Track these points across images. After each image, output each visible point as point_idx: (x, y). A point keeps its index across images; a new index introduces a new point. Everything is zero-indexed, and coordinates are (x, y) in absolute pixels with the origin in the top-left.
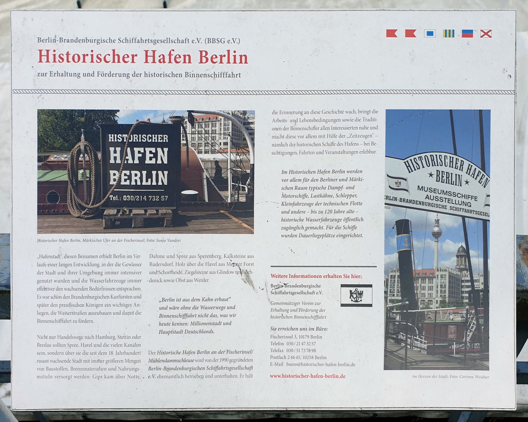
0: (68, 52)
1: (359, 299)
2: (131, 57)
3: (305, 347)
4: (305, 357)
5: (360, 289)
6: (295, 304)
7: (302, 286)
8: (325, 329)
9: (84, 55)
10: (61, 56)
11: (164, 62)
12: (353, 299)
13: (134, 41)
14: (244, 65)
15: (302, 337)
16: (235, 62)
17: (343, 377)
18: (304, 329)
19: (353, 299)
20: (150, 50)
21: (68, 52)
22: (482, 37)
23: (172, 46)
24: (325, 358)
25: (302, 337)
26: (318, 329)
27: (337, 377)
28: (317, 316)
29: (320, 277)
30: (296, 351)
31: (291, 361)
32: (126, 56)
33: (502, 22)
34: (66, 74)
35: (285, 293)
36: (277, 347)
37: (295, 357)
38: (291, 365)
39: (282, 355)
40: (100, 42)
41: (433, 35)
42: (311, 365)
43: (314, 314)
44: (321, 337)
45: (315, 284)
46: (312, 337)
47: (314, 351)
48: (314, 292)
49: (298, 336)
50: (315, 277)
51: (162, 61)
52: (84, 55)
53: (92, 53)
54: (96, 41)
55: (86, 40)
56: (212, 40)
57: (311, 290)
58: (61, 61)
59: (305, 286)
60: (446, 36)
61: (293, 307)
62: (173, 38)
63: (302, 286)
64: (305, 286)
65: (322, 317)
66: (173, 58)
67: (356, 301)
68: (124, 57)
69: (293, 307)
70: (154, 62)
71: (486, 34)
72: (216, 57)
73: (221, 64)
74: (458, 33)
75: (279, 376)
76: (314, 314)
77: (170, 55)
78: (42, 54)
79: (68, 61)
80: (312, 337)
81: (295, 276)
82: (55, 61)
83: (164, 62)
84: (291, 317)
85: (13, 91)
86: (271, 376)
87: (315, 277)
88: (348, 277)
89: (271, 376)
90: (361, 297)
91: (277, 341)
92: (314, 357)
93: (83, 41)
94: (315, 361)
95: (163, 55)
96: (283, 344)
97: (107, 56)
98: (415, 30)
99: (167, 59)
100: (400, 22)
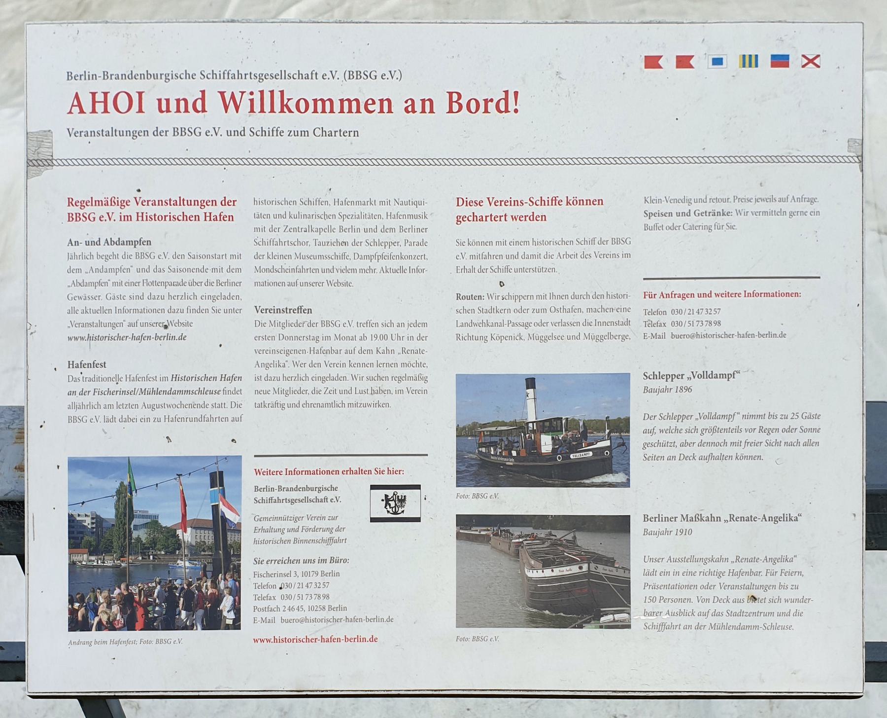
3: (312, 590)
4: (311, 609)
5: (400, 493)
6: (296, 519)
7: (307, 489)
8: (345, 561)
9: (486, 101)
11: (414, 111)
12: (390, 510)
13: (226, 76)
14: (428, 115)
15: (305, 574)
16: (272, 111)
17: (373, 640)
18: (310, 561)
19: (390, 510)
20: (99, 92)
22: (803, 66)
24: (345, 609)
25: (305, 574)
26: (333, 560)
27: (364, 640)
28: (331, 539)
29: (337, 472)
30: (296, 598)
31: (288, 615)
32: (370, 102)
33: (838, 44)
34: (113, 132)
35: (279, 500)
37: (296, 607)
38: (289, 621)
39: (272, 604)
40: (170, 77)
41: (722, 64)
42: (321, 620)
44: (338, 574)
45: (327, 486)
46: (323, 574)
47: (327, 597)
48: (326, 499)
49: (299, 574)
50: (328, 472)
51: (410, 109)
52: (486, 101)
54: (163, 77)
57: (321, 496)
59: (312, 489)
60: (744, 66)
61: (291, 525)
63: (307, 489)
64: (312, 489)
65: (339, 541)
67: (395, 513)
68: (366, 104)
69: (291, 525)
71: (811, 61)
73: (140, 114)
74: (765, 61)
75: (268, 641)
76: (326, 535)
78: (97, 100)
80: (323, 574)
81: (295, 472)
83: (414, 111)
84: (289, 541)
86: (256, 641)
87: (328, 472)
88: (382, 472)
89: (256, 641)
90: (402, 506)
92: (327, 608)
94: (330, 615)
95: (413, 101)
98: (661, 57)
100: (669, 42)
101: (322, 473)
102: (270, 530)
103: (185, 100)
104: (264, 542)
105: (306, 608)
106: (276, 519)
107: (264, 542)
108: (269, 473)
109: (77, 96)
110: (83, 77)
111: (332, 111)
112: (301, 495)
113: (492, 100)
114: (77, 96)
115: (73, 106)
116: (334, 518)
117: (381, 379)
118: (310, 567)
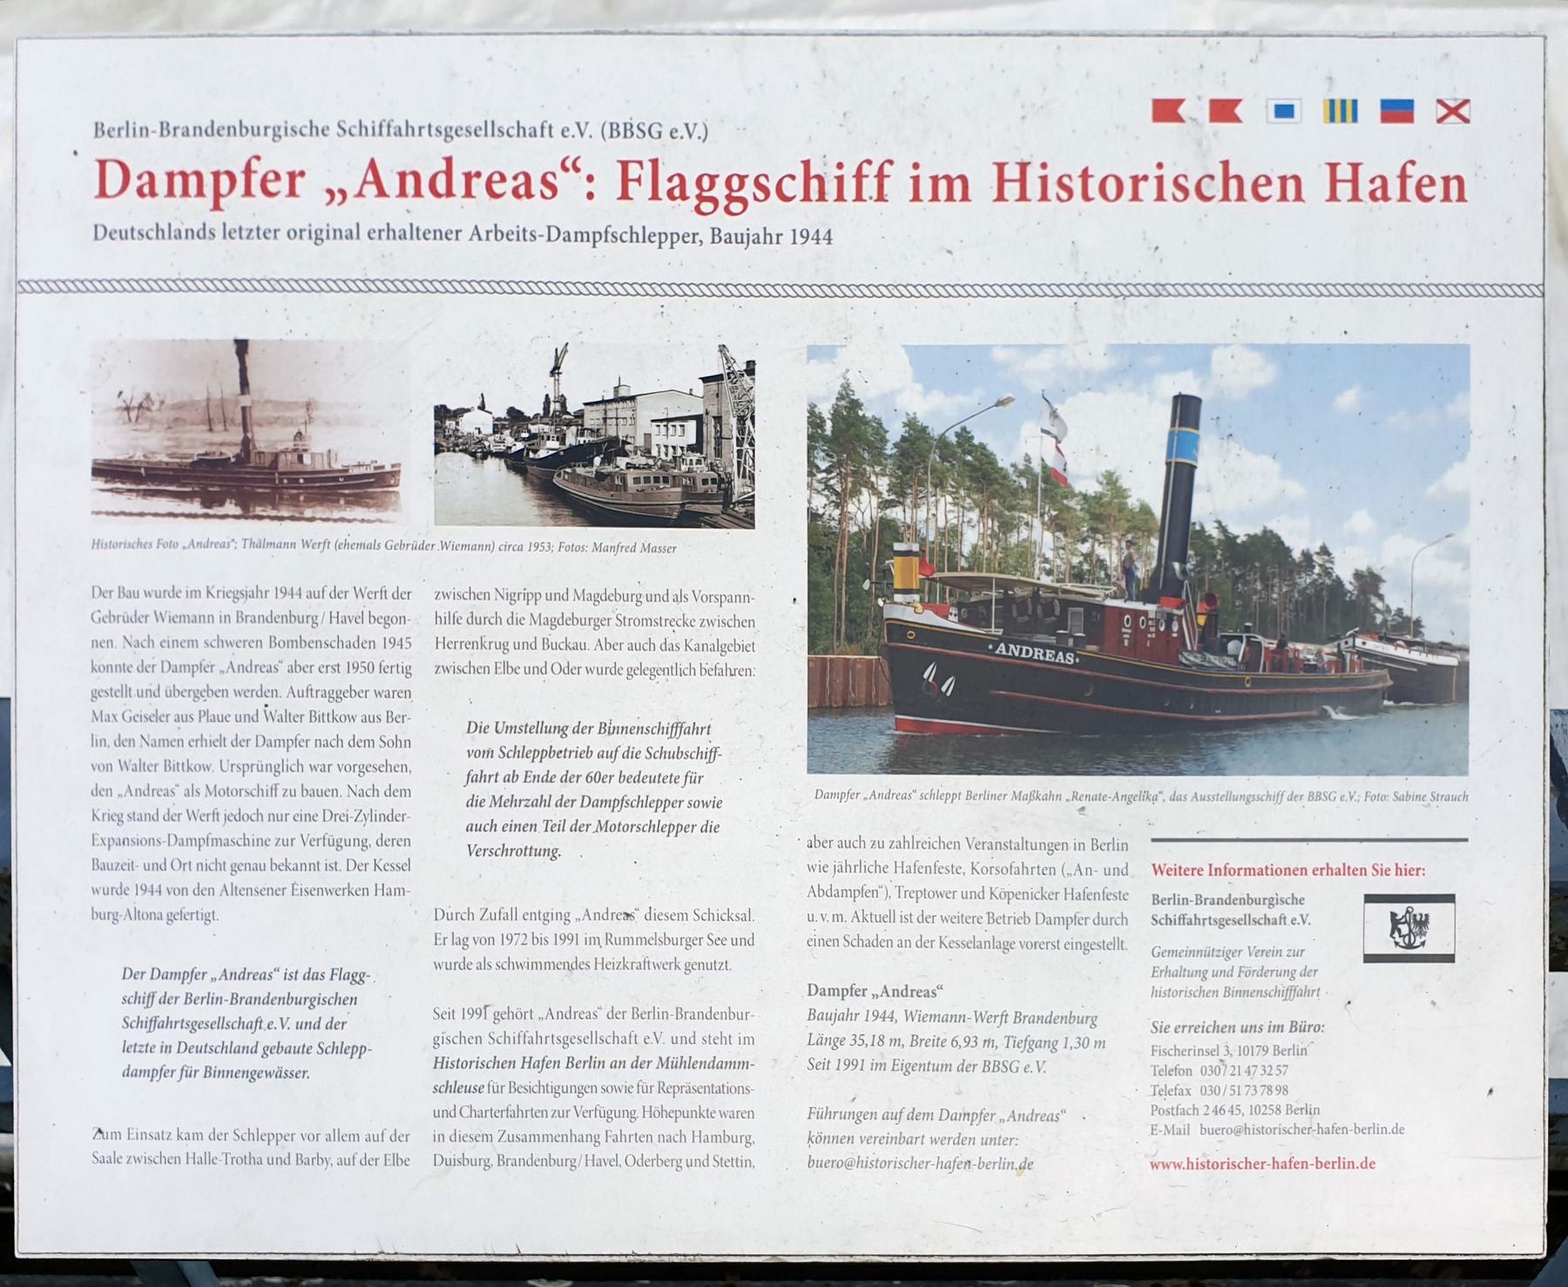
0: (1085, 170)
1: (1418, 941)
2: (285, 179)
3: (1259, 1079)
4: (1255, 1110)
5: (1419, 909)
6: (1228, 954)
8: (1318, 1028)
9: (1136, 180)
10: (1066, 181)
12: (1400, 940)
13: (385, 130)
15: (1245, 1051)
16: (840, 198)
17: (1368, 1164)
18: (1253, 1028)
19: (1400, 940)
21: (1085, 170)
22: (1440, 121)
23: (262, 144)
25: (1245, 1051)
27: (1351, 1165)
28: (1292, 989)
29: (1304, 871)
30: (1229, 1091)
31: (1214, 1122)
32: (1262, 181)
35: (1197, 921)
36: (1172, 1082)
37: (1227, 1108)
38: (1215, 1132)
39: (1185, 1102)
42: (1273, 1131)
43: (1285, 982)
46: (1278, 1051)
47: (1284, 1090)
48: (1283, 918)
50: (1288, 871)
51: (1379, 194)
52: (1136, 180)
53: (1159, 173)
54: (270, 132)
55: (241, 129)
56: (621, 129)
57: (1274, 913)
58: (1064, 195)
59: (1257, 902)
60: (1332, 119)
61: (1220, 964)
62: (504, 122)
64: (1257, 902)
65: (1307, 992)
66: (256, 180)
67: (1410, 946)
68: (1255, 185)
70: (1355, 197)
71: (1453, 111)
72: (1269, 182)
76: (1285, 982)
77: (1403, 176)
78: (1007, 176)
79: (1086, 197)
80: (1278, 1051)
81: (1226, 871)
82: (1044, 197)
83: (1386, 198)
84: (1216, 992)
85: (22, 286)
87: (1288, 871)
88: (1386, 872)
91: (1171, 1062)
92: (1283, 1109)
93: (231, 131)
94: (1287, 1121)
96: (1188, 1072)
97: (787, 181)
98: (1237, 102)
99: (1394, 189)
101: (1275, 872)
102: (1181, 973)
103: (416, 175)
104: (1168, 993)
105: (1245, 1110)
106: (1191, 953)
107: (1168, 993)
108: (1180, 871)
109: (372, 165)
110: (123, 133)
111: (822, 197)
112: (1238, 911)
113: (478, 175)
114: (372, 165)
115: (365, 182)
116: (1298, 953)
117: (477, 597)
118: (1255, 1039)
